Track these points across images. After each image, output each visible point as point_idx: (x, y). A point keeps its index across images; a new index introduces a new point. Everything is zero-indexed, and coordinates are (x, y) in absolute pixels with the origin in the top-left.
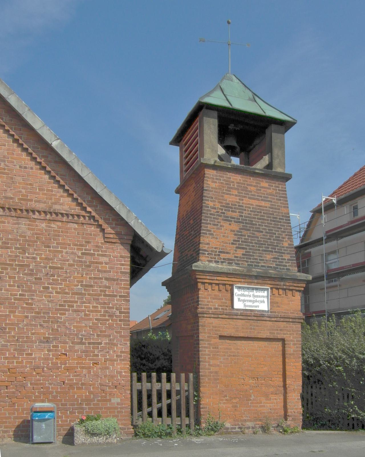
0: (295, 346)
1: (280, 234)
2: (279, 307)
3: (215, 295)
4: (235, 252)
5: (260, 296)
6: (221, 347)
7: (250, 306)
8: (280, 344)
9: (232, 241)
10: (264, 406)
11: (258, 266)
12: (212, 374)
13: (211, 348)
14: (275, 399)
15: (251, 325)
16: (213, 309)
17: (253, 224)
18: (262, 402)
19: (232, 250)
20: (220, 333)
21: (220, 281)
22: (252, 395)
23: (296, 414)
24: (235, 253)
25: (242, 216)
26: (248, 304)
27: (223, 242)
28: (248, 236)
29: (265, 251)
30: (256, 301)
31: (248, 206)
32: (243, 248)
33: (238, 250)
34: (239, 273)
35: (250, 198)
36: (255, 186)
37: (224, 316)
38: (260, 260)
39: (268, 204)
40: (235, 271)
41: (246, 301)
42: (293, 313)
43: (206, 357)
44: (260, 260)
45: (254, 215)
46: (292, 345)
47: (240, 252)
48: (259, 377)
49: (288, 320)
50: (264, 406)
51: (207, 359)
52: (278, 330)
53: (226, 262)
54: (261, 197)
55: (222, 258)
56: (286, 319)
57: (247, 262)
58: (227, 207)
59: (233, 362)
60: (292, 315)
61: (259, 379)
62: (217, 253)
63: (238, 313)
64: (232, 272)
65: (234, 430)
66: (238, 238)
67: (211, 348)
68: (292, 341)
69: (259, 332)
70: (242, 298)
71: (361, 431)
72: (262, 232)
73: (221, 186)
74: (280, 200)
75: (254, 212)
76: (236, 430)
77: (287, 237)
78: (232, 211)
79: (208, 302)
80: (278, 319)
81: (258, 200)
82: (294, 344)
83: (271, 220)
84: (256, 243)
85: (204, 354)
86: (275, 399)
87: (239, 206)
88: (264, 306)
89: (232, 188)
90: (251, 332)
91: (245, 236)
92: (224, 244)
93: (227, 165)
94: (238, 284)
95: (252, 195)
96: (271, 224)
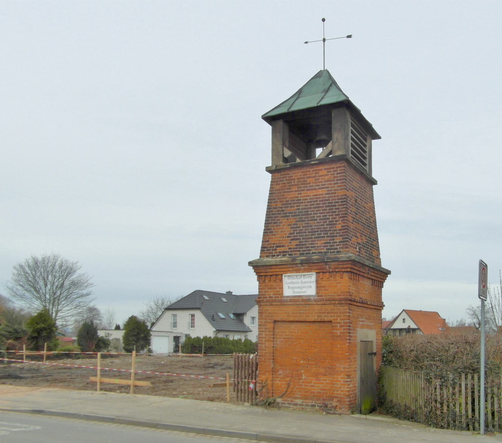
2: (326, 290)
3: (271, 286)
8: (279, 325)
10: (314, 386)
14: (324, 380)
15: (300, 310)
22: (303, 375)
25: (299, 209)
26: (296, 290)
28: (303, 227)
30: (304, 287)
32: (297, 239)
33: (293, 241)
34: (285, 263)
35: (308, 190)
36: (313, 177)
37: (277, 303)
38: (312, 247)
39: (324, 191)
44: (312, 247)
45: (310, 205)
46: (339, 327)
47: (294, 243)
49: (334, 302)
50: (314, 386)
52: (325, 313)
54: (319, 185)
57: (299, 251)
64: (278, 263)
68: (339, 323)
70: (291, 286)
71: (498, 434)
72: (317, 220)
74: (337, 183)
78: (291, 207)
81: (315, 189)
82: (341, 326)
83: (326, 206)
84: (309, 232)
86: (324, 380)
87: (298, 200)
89: (292, 185)
91: (300, 227)
96: (326, 210)
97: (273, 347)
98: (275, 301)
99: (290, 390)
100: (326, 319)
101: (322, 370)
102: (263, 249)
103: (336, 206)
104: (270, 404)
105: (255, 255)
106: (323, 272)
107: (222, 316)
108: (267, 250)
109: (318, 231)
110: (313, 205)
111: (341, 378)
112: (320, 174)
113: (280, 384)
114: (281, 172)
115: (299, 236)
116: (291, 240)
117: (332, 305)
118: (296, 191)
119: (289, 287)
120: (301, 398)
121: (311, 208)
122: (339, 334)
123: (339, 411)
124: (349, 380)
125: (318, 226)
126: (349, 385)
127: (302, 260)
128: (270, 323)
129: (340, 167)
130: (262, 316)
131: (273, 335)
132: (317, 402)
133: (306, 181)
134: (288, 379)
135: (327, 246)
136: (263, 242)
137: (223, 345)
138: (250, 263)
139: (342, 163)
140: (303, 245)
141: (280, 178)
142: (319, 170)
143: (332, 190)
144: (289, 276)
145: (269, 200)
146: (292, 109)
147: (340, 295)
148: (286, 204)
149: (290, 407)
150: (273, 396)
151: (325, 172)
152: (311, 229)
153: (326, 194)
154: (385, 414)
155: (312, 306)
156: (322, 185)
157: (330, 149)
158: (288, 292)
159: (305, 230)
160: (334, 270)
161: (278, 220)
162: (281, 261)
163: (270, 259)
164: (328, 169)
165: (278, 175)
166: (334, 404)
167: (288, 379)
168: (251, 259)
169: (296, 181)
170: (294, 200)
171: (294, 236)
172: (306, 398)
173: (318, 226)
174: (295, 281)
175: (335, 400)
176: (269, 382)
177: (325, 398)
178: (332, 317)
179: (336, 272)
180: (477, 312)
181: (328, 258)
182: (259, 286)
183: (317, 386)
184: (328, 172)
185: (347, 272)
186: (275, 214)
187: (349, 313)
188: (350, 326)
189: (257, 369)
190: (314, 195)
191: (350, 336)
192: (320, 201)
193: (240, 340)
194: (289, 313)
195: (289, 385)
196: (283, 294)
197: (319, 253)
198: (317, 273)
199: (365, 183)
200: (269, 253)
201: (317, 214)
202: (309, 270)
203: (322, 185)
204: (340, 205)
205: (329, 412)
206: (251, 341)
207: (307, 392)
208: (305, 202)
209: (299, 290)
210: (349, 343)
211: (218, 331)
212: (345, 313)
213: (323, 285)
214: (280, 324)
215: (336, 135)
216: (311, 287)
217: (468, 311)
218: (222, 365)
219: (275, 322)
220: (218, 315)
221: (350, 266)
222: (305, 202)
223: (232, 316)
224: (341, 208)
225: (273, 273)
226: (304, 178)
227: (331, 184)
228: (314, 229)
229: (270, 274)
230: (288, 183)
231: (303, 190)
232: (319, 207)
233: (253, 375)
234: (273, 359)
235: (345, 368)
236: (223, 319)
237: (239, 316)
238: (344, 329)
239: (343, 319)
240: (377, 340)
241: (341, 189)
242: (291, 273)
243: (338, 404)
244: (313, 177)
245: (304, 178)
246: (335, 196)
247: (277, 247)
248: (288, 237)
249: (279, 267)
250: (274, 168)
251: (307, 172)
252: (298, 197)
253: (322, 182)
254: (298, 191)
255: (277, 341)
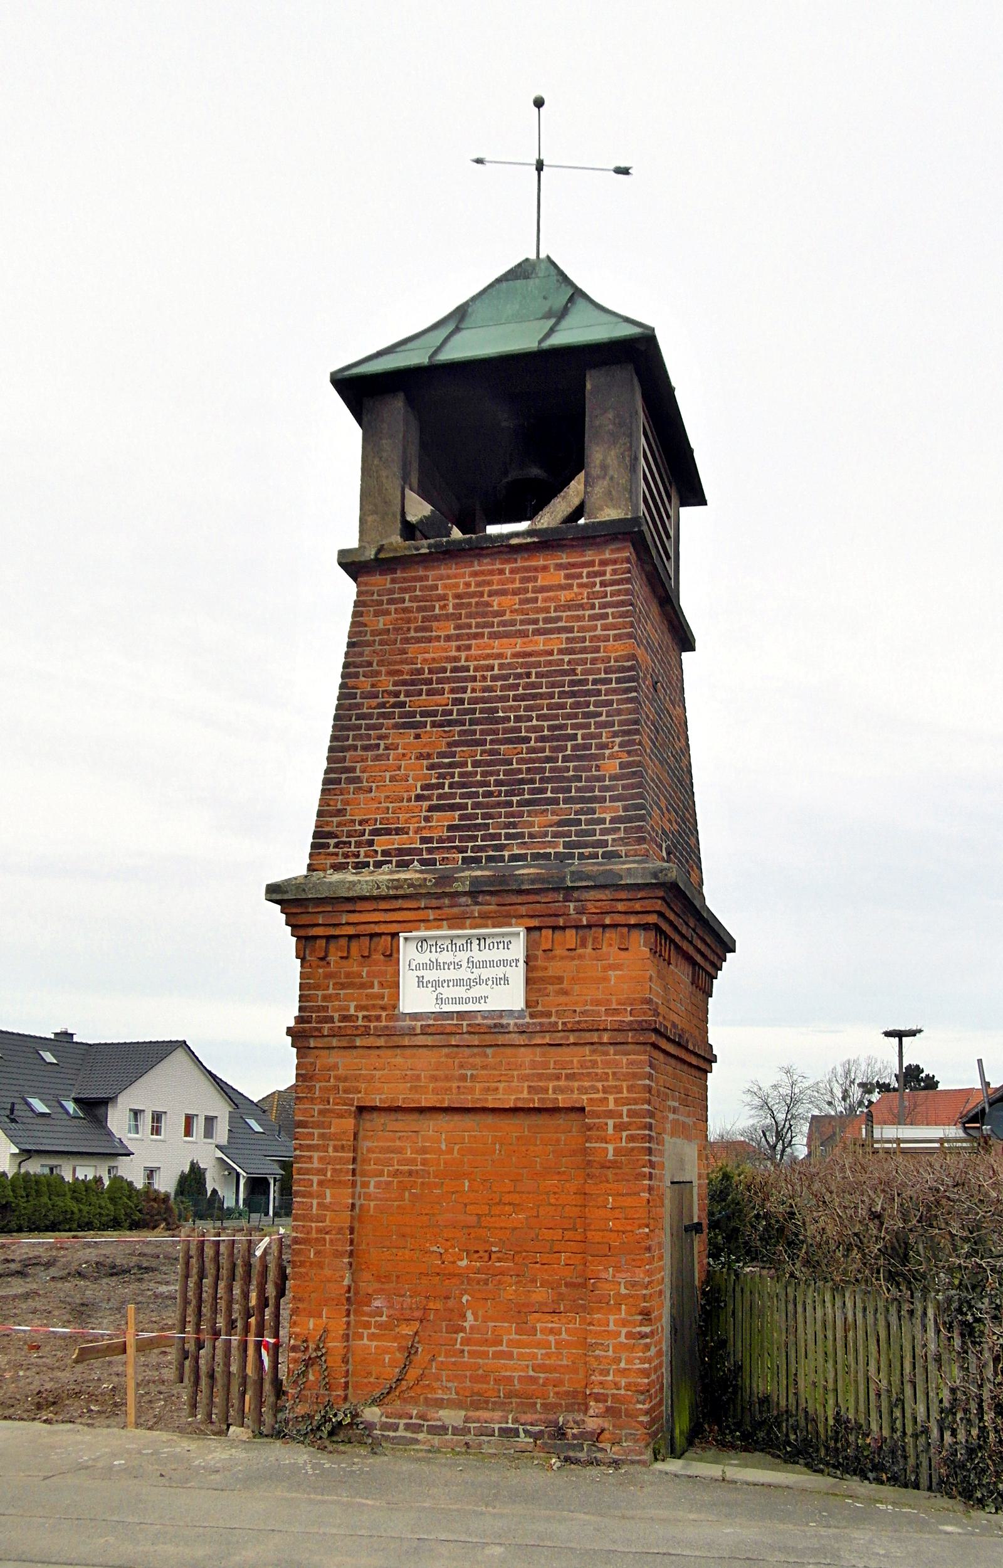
0: (624, 1134)
1: (592, 736)
2: (566, 993)
4: (423, 824)
5: (492, 964)
6: (370, 1144)
7: (457, 999)
9: (419, 791)
10: (510, 1356)
11: (501, 859)
12: (327, 1237)
13: (330, 1149)
14: (551, 1331)
15: (461, 1066)
16: (336, 1020)
17: (497, 721)
18: (502, 1341)
19: (415, 820)
20: (358, 1099)
21: (362, 927)
22: (469, 1315)
23: (622, 1392)
24: (424, 828)
25: (461, 701)
26: (448, 992)
27: (388, 797)
28: (476, 764)
29: (528, 803)
30: (479, 981)
31: (487, 662)
32: (453, 808)
35: (494, 636)
36: (515, 593)
38: (508, 836)
39: (558, 641)
40: (396, 888)
41: (445, 985)
42: (616, 1012)
43: (312, 1181)
44: (508, 836)
46: (610, 1131)
47: (442, 821)
48: (494, 1249)
51: (315, 1185)
52: (558, 1078)
53: (390, 862)
54: (535, 622)
55: (379, 849)
56: (584, 1032)
58: (414, 682)
59: (407, 1194)
60: (609, 1020)
61: (493, 1256)
62: (367, 837)
63: (414, 1029)
64: (384, 891)
65: (392, 1434)
66: (438, 778)
67: (330, 1149)
68: (610, 1114)
69: (488, 1089)
70: (430, 975)
72: (527, 740)
73: (401, 619)
74: (605, 616)
75: (505, 677)
76: (398, 1434)
77: (618, 740)
78: (429, 693)
79: (325, 998)
80: (558, 1038)
81: (523, 634)
82: (619, 1128)
83: (562, 694)
84: (499, 783)
85: (307, 1169)
86: (551, 1331)
88: (510, 997)
89: (437, 618)
90: (462, 1090)
92: (391, 805)
93: (417, 549)
94: (418, 929)
95: (503, 624)
96: (563, 706)
97: (353, 1205)
98: (366, 1032)
99: (413, 1373)
100: (562, 1100)
101: (540, 1294)
102: (321, 840)
103: (598, 693)
104: (334, 1431)
105: (292, 862)
106: (554, 928)
107: (40, 1107)
108: (336, 846)
109: (533, 781)
110: (515, 687)
111: (616, 1324)
112: (539, 583)
113: (377, 1349)
114: (394, 571)
115: (463, 796)
116: (431, 809)
117: (587, 1049)
118: (448, 638)
119: (420, 982)
120: (458, 1405)
121: (505, 699)
122: (610, 1156)
123: (614, 1452)
124: (647, 1329)
125: (533, 761)
126: (647, 1347)
127: (475, 881)
128: (341, 1116)
129: (615, 562)
130: (311, 1089)
131: (354, 1160)
132: (525, 1418)
133: (488, 604)
134: (407, 1330)
135: (568, 834)
136: (320, 814)
137: (45, 1199)
138: (275, 892)
139: (619, 550)
140: (477, 827)
141: (391, 591)
142: (536, 569)
143: (584, 640)
144: (424, 940)
145: (346, 665)
146: (445, 356)
147: (616, 1012)
148: (413, 683)
149: (417, 1441)
150: (346, 1398)
151: (560, 578)
152: (506, 773)
153: (561, 652)
154: (746, 1449)
155: (508, 1050)
156: (547, 620)
157: (576, 502)
158: (415, 999)
159: (484, 774)
160: (595, 919)
161: (380, 738)
162: (397, 884)
163: (349, 876)
164: (573, 565)
165: (381, 582)
166: (592, 1424)
167: (407, 1330)
168: (278, 876)
169: (452, 602)
170: (444, 670)
171: (440, 797)
172: (478, 1402)
173: (533, 761)
174: (446, 957)
175: (595, 1407)
176: (335, 1344)
177: (552, 1399)
178: (582, 1090)
179: (605, 926)
180: (771, 1102)
181: (578, 875)
182: (303, 975)
183: (521, 1356)
184: (567, 577)
185: (646, 927)
186: (369, 716)
187: (650, 1077)
188: (650, 1127)
189: (281, 1293)
190: (516, 655)
191: (652, 1165)
192: (538, 675)
193: (98, 1180)
194: (418, 1078)
195: (410, 1352)
196: (395, 1006)
197: (536, 856)
198: (529, 929)
199: (668, 639)
200: (346, 856)
201: (530, 719)
202: (501, 919)
203: (547, 620)
204: (614, 691)
205: (571, 1454)
206: (130, 1184)
207: (484, 1379)
208: (484, 678)
209: (460, 992)
210: (650, 1189)
211: (27, 1154)
212: (635, 1076)
213: (550, 973)
214: (379, 1120)
215: (598, 454)
216: (506, 980)
217: (748, 1098)
218: (48, 1265)
219: (361, 1110)
220: (28, 1104)
221: (659, 905)
222: (484, 678)
223: (71, 1106)
224: (619, 702)
225: (361, 929)
226: (482, 594)
227: (580, 618)
228: (520, 771)
229: (351, 931)
230: (420, 609)
231: (476, 636)
232: (534, 697)
233: (263, 1316)
234: (351, 1254)
235: (634, 1284)
236: (43, 1115)
237: (94, 1108)
238: (631, 1139)
239: (627, 1102)
240: (700, 1177)
241: (617, 638)
242: (427, 929)
243: (606, 1424)
244: (515, 593)
245: (482, 594)
246: (594, 661)
247: (376, 832)
248: (419, 798)
249: (383, 905)
250: (371, 554)
251: (491, 573)
252: (456, 659)
253: (547, 610)
254: (458, 637)
255: (365, 1185)
